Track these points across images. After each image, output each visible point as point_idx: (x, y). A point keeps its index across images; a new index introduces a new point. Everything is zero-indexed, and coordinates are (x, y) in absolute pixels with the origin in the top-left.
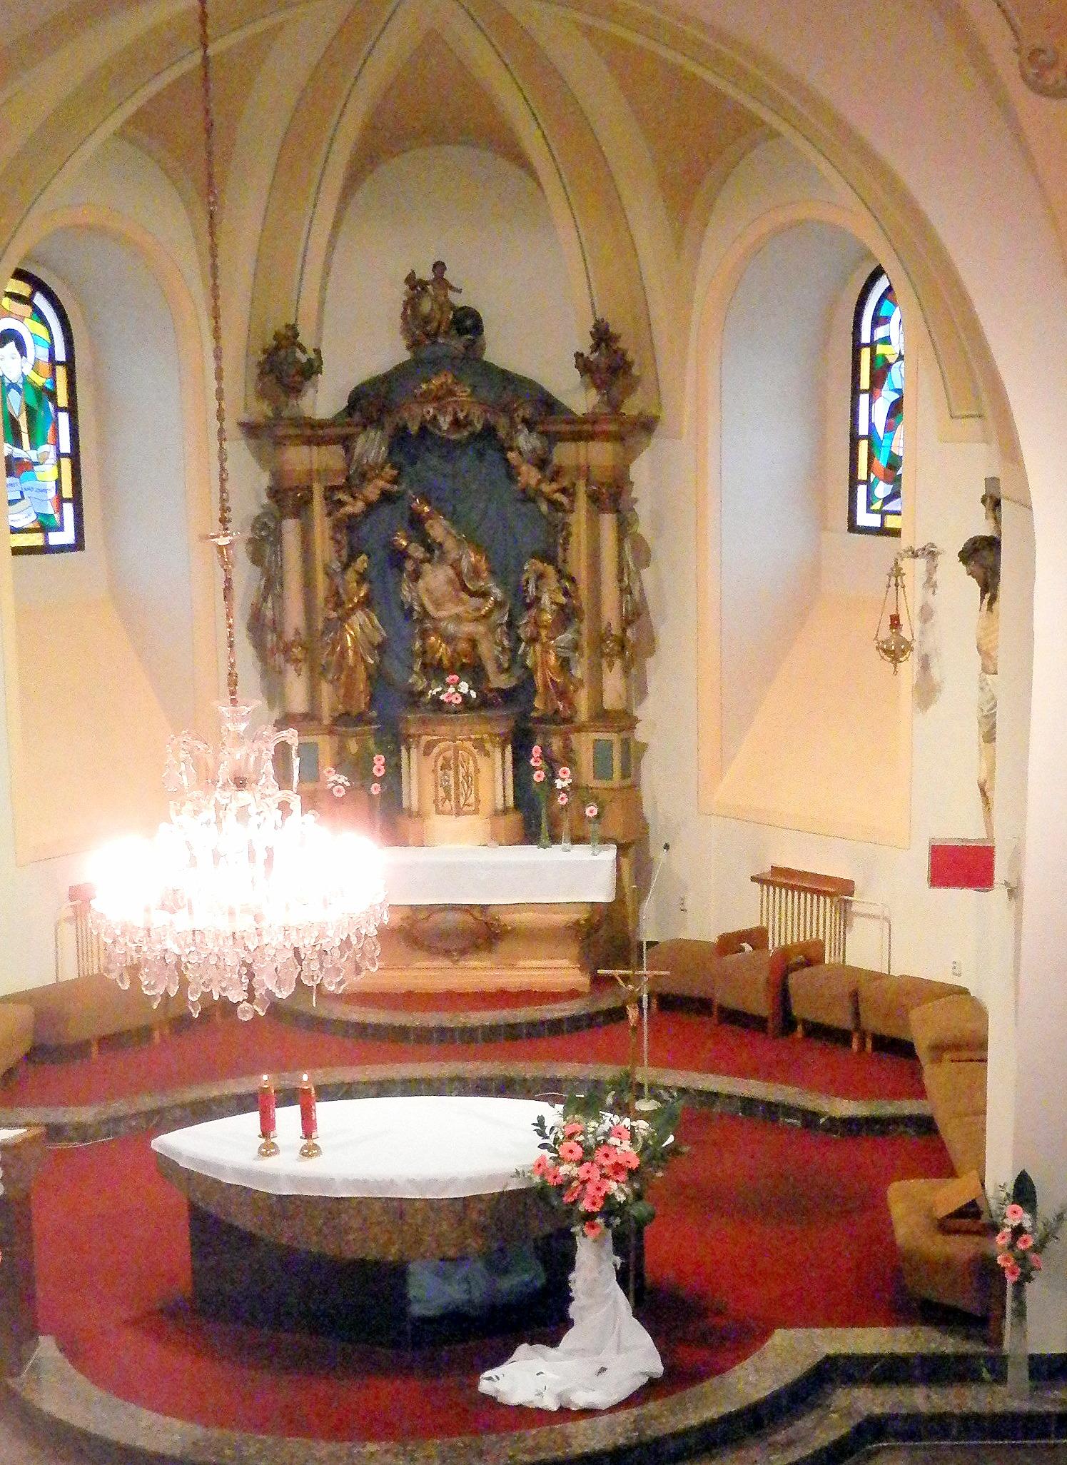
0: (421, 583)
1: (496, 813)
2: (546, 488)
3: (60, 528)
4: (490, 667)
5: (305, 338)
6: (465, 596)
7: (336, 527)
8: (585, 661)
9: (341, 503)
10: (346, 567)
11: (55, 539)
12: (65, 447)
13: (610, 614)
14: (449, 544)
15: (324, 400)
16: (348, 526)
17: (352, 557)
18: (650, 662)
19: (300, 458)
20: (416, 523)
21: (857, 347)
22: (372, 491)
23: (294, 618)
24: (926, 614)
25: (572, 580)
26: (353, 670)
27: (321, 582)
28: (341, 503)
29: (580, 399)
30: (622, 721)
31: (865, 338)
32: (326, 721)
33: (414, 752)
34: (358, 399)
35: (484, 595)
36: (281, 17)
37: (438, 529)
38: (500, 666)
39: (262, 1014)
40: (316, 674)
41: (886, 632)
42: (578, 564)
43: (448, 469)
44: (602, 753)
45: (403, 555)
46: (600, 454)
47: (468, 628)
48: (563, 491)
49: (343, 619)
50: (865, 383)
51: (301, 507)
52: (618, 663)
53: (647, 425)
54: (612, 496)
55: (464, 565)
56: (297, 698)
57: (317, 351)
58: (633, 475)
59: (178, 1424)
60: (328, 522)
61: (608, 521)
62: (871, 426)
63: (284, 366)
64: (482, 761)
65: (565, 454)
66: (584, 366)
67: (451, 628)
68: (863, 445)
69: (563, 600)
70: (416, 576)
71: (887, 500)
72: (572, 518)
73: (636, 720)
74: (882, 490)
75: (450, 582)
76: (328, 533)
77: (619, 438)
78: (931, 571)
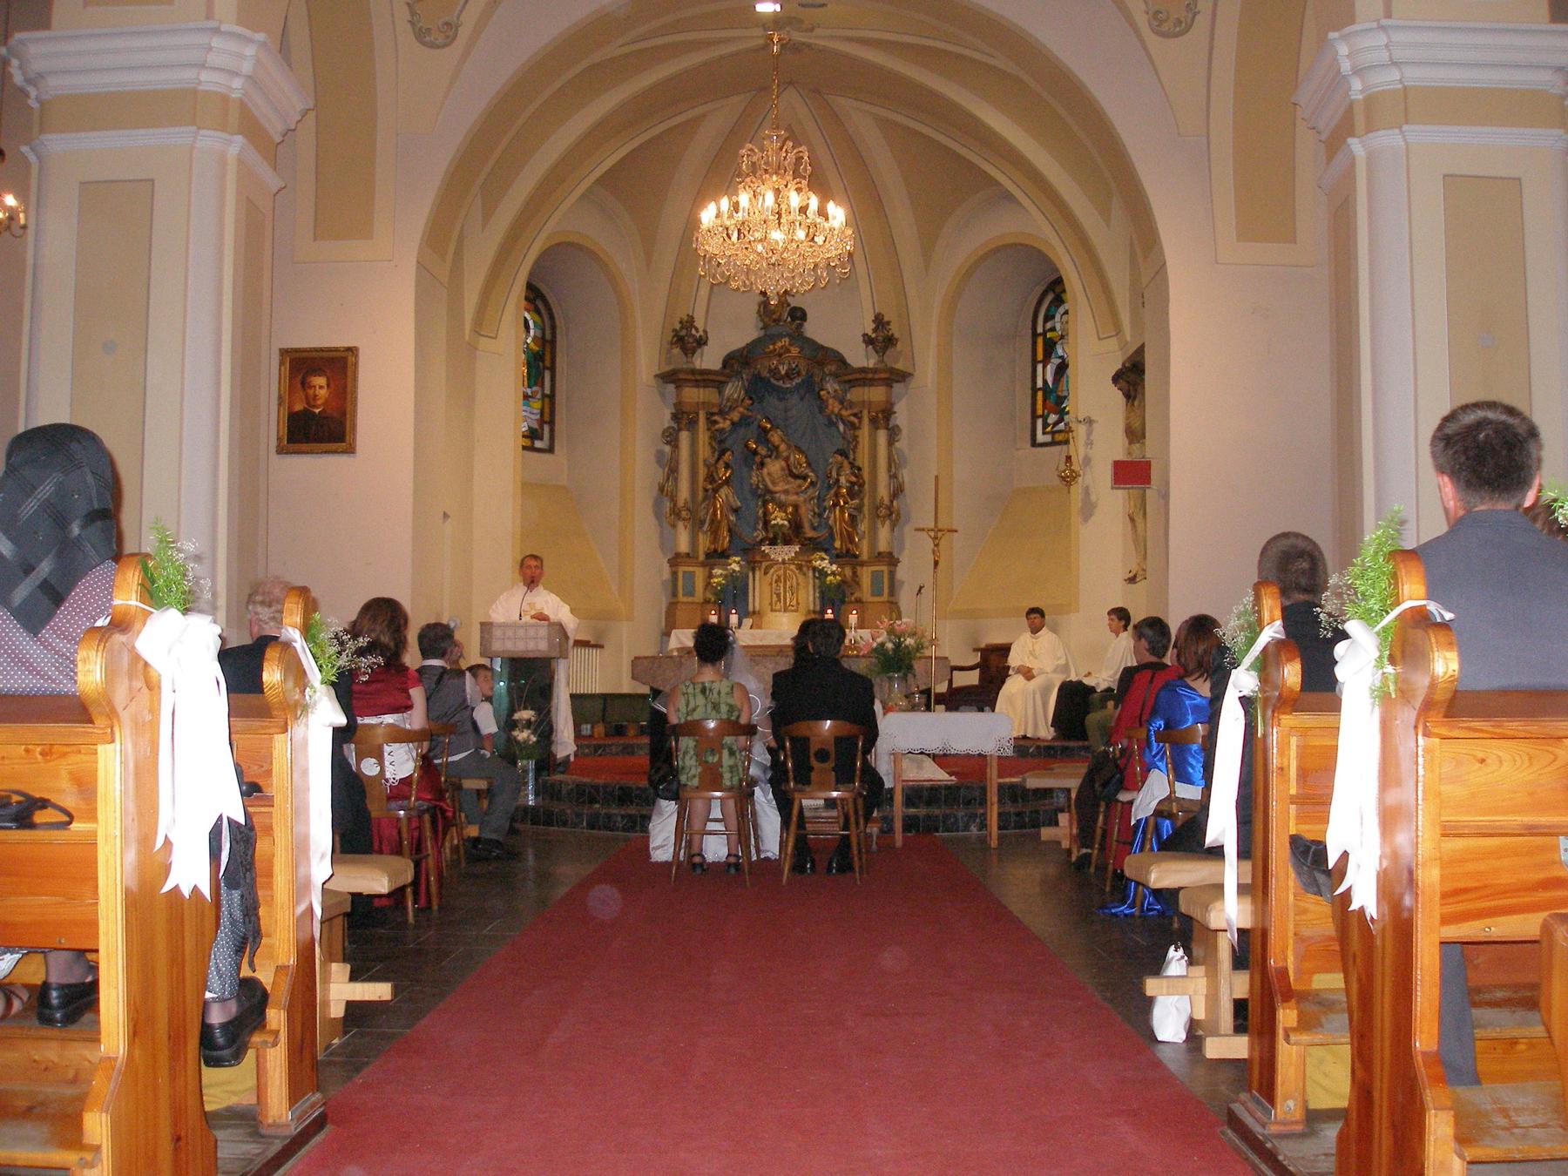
3: (541, 439)
4: (806, 525)
5: (699, 323)
9: (716, 422)
11: (538, 444)
12: (547, 391)
13: (883, 492)
14: (783, 447)
15: (710, 359)
16: (720, 444)
17: (722, 453)
19: (692, 395)
21: (1035, 335)
22: (735, 416)
23: (684, 493)
24: (1087, 461)
25: (859, 469)
27: (702, 472)
28: (716, 422)
29: (859, 357)
30: (891, 560)
31: (1040, 330)
32: (702, 557)
34: (728, 361)
35: (805, 478)
36: (699, 110)
37: (775, 437)
40: (696, 525)
41: (1062, 467)
42: (863, 459)
44: (876, 578)
45: (755, 452)
46: (876, 394)
47: (793, 498)
48: (855, 415)
49: (716, 491)
50: (1040, 357)
51: (692, 424)
53: (903, 377)
56: (683, 545)
57: (705, 332)
59: (736, 99)
60: (708, 434)
61: (882, 436)
62: (1045, 381)
63: (686, 339)
64: (801, 578)
65: (855, 394)
66: (868, 341)
67: (783, 497)
68: (1040, 394)
69: (854, 479)
70: (762, 465)
71: (1056, 424)
72: (858, 433)
74: (1053, 418)
78: (1089, 433)
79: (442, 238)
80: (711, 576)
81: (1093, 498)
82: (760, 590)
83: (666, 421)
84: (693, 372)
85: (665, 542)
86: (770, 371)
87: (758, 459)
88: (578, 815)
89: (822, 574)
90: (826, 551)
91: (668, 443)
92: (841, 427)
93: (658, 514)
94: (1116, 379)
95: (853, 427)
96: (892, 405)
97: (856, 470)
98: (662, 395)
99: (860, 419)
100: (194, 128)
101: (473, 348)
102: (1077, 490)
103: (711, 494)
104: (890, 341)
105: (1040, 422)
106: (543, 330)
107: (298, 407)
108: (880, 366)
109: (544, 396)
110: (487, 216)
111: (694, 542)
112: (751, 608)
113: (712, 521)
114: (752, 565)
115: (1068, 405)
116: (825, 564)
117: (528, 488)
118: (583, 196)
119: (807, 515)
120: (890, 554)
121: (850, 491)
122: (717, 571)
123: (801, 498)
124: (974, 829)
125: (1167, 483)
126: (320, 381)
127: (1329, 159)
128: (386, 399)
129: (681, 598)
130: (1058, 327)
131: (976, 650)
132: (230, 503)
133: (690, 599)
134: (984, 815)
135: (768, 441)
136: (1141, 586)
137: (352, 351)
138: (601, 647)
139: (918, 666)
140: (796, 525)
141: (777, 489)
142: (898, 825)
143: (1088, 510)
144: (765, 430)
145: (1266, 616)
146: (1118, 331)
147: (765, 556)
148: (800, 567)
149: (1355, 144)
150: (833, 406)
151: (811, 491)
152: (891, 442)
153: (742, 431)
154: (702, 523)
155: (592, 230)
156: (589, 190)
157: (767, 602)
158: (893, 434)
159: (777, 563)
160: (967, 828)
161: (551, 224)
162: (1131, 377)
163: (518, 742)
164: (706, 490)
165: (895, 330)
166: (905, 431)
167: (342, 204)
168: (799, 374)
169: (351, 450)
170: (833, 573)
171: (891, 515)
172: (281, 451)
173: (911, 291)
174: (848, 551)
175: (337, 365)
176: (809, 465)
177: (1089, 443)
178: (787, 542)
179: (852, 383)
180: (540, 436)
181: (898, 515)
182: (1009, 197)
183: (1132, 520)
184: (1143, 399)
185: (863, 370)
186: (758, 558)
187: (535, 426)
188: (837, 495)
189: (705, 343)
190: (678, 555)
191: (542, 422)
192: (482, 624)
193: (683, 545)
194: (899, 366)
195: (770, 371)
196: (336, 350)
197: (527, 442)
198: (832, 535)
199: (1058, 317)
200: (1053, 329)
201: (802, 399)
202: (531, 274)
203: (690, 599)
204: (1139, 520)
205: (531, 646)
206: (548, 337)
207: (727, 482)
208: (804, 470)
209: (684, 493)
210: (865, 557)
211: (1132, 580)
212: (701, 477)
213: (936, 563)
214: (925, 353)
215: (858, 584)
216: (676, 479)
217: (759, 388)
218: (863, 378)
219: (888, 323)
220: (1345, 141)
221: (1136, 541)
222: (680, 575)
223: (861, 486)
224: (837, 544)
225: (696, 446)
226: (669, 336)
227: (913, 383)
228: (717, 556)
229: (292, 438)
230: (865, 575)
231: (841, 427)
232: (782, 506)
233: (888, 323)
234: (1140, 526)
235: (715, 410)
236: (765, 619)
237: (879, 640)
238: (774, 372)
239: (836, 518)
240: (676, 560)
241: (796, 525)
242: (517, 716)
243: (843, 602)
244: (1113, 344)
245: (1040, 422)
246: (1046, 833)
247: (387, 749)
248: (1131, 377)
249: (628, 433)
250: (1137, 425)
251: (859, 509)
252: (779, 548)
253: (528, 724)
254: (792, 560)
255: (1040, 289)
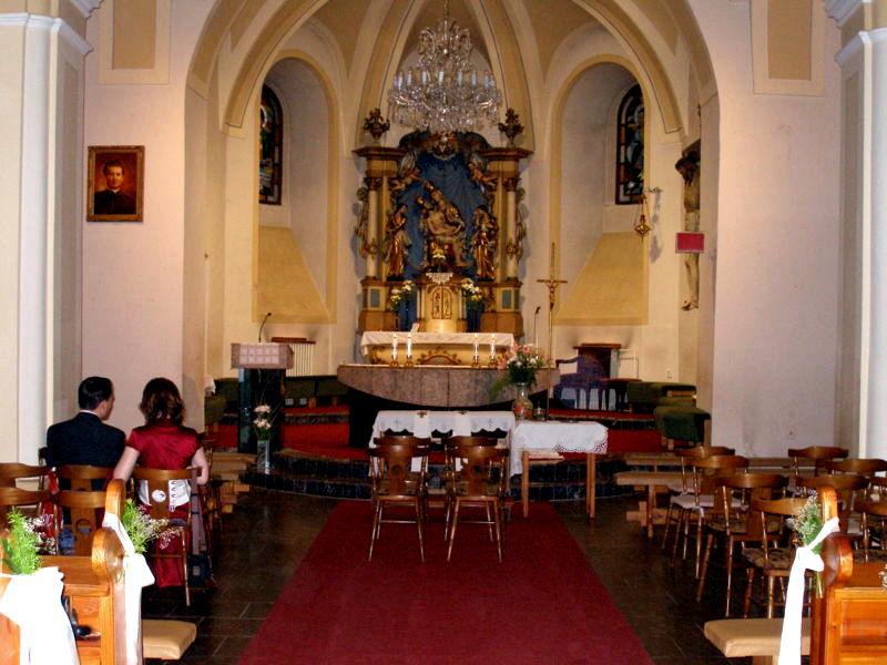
0: (429, 220)
1: (459, 319)
2: (485, 179)
3: (272, 195)
4: (458, 257)
6: (447, 226)
7: (393, 196)
8: (499, 256)
9: (395, 185)
10: (396, 212)
12: (276, 161)
13: (512, 235)
14: (442, 203)
15: (391, 140)
16: (397, 198)
18: (528, 261)
20: (428, 196)
21: (620, 126)
23: (372, 234)
24: (656, 218)
25: (495, 219)
26: (397, 256)
27: (385, 220)
28: (395, 185)
29: (496, 139)
30: (516, 283)
31: (623, 122)
32: (384, 280)
33: (423, 292)
34: (404, 141)
35: (457, 225)
37: (437, 196)
38: (461, 257)
39: (712, 505)
40: (381, 257)
41: (638, 223)
42: (498, 211)
43: (441, 173)
45: (422, 207)
46: (508, 166)
47: (448, 239)
48: (493, 181)
49: (394, 233)
51: (378, 187)
52: (514, 257)
53: (526, 154)
54: (512, 183)
55: (448, 212)
56: (372, 272)
57: (388, 121)
58: (521, 176)
61: (511, 196)
64: (453, 296)
65: (494, 166)
66: (502, 128)
67: (442, 238)
68: (622, 167)
69: (491, 226)
70: (427, 216)
72: (495, 193)
73: (521, 284)
74: (631, 185)
75: (441, 218)
76: (389, 197)
77: (516, 159)
78: (658, 199)
79: (203, 67)
80: (390, 294)
81: (659, 244)
82: (424, 304)
83: (361, 184)
84: (380, 149)
85: (359, 268)
86: (433, 148)
87: (424, 211)
88: (301, 483)
89: (469, 293)
90: (471, 277)
91: (361, 199)
92: (483, 189)
93: (353, 247)
94: (678, 166)
95: (490, 189)
96: (519, 174)
97: (493, 219)
98: (358, 165)
99: (496, 183)
100: (26, 15)
101: (225, 134)
102: (648, 239)
103: (391, 236)
104: (518, 129)
105: (622, 187)
106: (274, 118)
107: (102, 188)
108: (511, 146)
109: (274, 165)
110: (234, 44)
111: (379, 267)
112: (418, 316)
113: (392, 255)
114: (419, 286)
115: (645, 176)
116: (470, 286)
117: (263, 230)
118: (304, 25)
119: (458, 251)
120: (516, 279)
121: (488, 234)
122: (396, 291)
123: (454, 240)
124: (576, 496)
125: (715, 251)
126: (117, 170)
127: (844, 44)
128: (164, 182)
129: (370, 308)
130: (636, 120)
131: (575, 348)
132: (56, 198)
133: (376, 309)
134: (585, 486)
135: (431, 198)
136: (693, 311)
137: (141, 149)
138: (314, 343)
139: (539, 376)
140: (450, 257)
141: (438, 232)
142: (525, 495)
143: (655, 253)
144: (430, 192)
145: (826, 514)
146: (680, 129)
147: (429, 280)
148: (453, 288)
149: (865, 36)
150: (478, 175)
151: (461, 234)
152: (517, 201)
153: (413, 191)
154: (385, 256)
155: (310, 50)
156: (308, 22)
157: (429, 311)
158: (519, 195)
159: (437, 285)
160: (572, 496)
161: (281, 46)
162: (690, 164)
163: (258, 429)
164: (388, 233)
165: (522, 121)
166: (527, 193)
167: (134, 48)
168: (453, 151)
169: (139, 219)
170: (476, 294)
171: (518, 251)
172: (90, 219)
173: (534, 94)
174: (487, 276)
175: (131, 158)
176: (459, 214)
177: (657, 206)
178: (444, 270)
179: (492, 158)
180: (270, 192)
181: (522, 252)
182: (602, 28)
183: (688, 266)
184: (698, 182)
185: (499, 150)
186: (424, 281)
187: (269, 186)
188: (480, 237)
189: (388, 129)
190: (367, 278)
191: (272, 183)
192: (233, 345)
193: (372, 272)
194: (524, 146)
195: (433, 148)
196: (129, 148)
197: (264, 197)
198: (475, 265)
199: (636, 113)
200: (633, 122)
201: (455, 168)
202: (268, 78)
203: (376, 309)
204: (693, 266)
205: (268, 360)
206: (277, 122)
207: (403, 227)
208: (456, 219)
209: (372, 234)
210: (498, 280)
211: (687, 308)
212: (384, 224)
213: (552, 305)
214: (543, 134)
215: (493, 299)
216: (366, 225)
217: (425, 161)
218: (500, 155)
219: (517, 116)
220: (857, 32)
221: (690, 281)
222: (369, 291)
223: (497, 231)
224: (479, 272)
225: (381, 202)
226: (363, 124)
227: (534, 158)
228: (395, 280)
229: (97, 211)
230: (499, 294)
231: (483, 189)
232: (441, 245)
233: (517, 116)
234: (694, 271)
235: (395, 176)
236: (428, 324)
237: (512, 360)
238: (436, 150)
239: (479, 254)
240: (366, 282)
241: (450, 257)
242: (257, 410)
243: (483, 312)
244: (675, 137)
245: (622, 187)
246: (631, 515)
247: (171, 486)
248: (690, 164)
249: (332, 197)
250: (693, 199)
251: (495, 247)
252: (438, 275)
253: (265, 415)
254: (447, 284)
255: (624, 93)
